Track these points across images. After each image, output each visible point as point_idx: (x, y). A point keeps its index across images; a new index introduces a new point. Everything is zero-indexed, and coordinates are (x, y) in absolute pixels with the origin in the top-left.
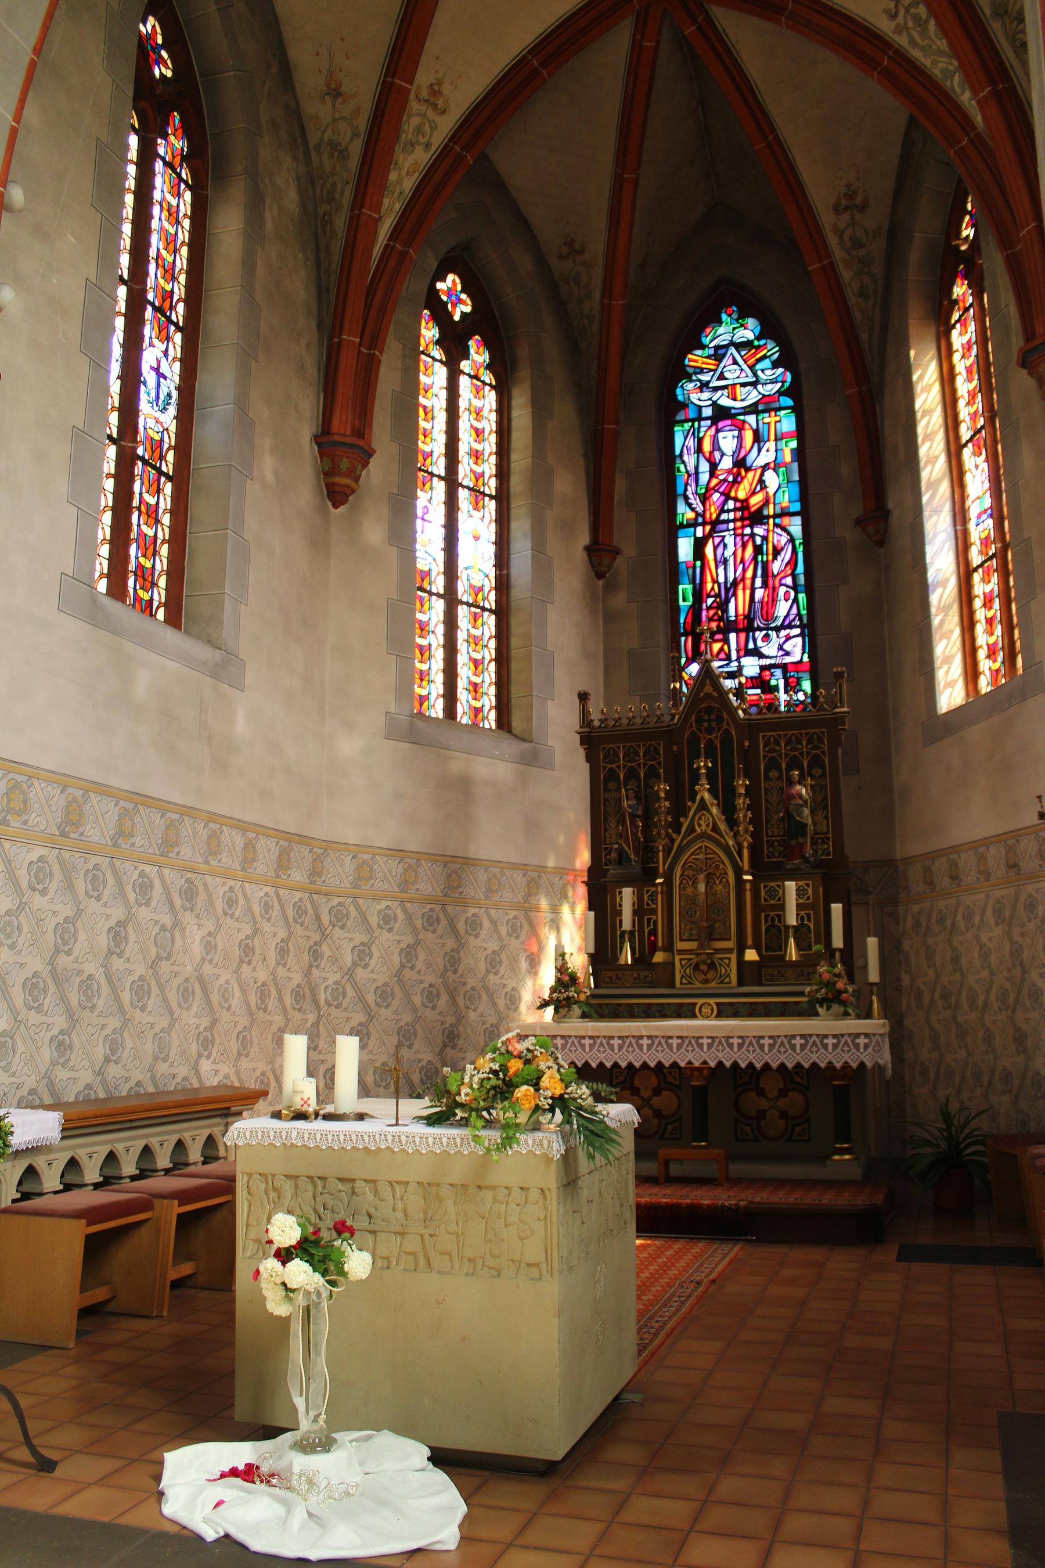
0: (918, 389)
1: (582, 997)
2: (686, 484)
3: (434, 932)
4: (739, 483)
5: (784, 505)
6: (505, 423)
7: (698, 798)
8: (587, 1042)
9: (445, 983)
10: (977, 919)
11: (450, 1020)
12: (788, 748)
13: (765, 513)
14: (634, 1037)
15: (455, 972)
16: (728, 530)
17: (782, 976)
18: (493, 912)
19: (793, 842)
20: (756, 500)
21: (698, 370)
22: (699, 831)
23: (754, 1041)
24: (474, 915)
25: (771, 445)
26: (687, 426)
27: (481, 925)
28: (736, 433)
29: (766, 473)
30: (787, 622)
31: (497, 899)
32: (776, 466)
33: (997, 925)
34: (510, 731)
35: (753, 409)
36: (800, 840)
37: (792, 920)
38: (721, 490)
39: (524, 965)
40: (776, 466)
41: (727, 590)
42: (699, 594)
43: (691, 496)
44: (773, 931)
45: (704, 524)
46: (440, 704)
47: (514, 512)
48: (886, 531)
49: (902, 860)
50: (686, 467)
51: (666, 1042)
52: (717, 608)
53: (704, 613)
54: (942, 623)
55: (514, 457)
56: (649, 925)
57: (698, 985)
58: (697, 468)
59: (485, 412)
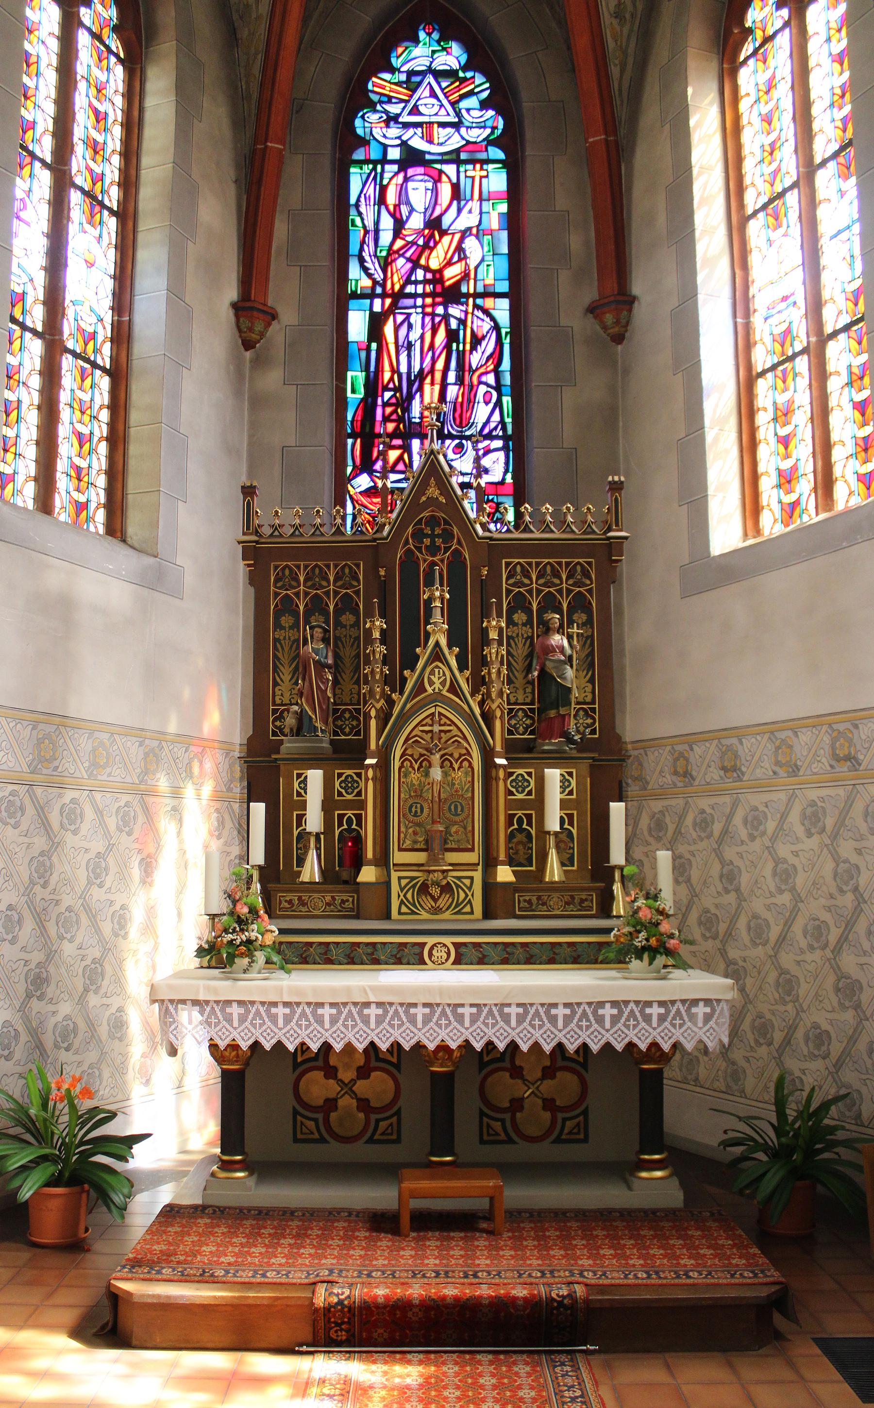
0: (696, 137)
1: (269, 939)
2: (363, 242)
3: (16, 826)
4: (432, 249)
5: (487, 282)
6: (136, 113)
7: (431, 642)
8: (235, 1011)
9: (30, 904)
10: (771, 826)
11: (37, 957)
12: (541, 581)
13: (464, 289)
14: (355, 1004)
15: (45, 886)
16: (415, 307)
17: (544, 904)
18: (98, 796)
19: (552, 713)
20: (452, 273)
21: (385, 99)
22: (430, 690)
23: (542, 1011)
24: (73, 801)
25: (475, 205)
26: (367, 168)
27: (82, 815)
28: (430, 185)
29: (467, 240)
30: (486, 431)
31: (105, 777)
32: (480, 232)
33: (809, 835)
34: (124, 541)
35: (454, 157)
36: (562, 711)
37: (553, 824)
38: (408, 255)
39: (136, 872)
40: (480, 232)
41: (410, 384)
42: (373, 386)
43: (367, 258)
44: (520, 837)
45: (383, 296)
46: (30, 490)
47: (142, 238)
48: (628, 323)
49: (633, 742)
50: (362, 220)
51: (406, 1012)
52: (396, 405)
53: (379, 411)
54: (716, 440)
55: (146, 161)
56: (340, 824)
57: (425, 915)
58: (377, 223)
59: (109, 91)
